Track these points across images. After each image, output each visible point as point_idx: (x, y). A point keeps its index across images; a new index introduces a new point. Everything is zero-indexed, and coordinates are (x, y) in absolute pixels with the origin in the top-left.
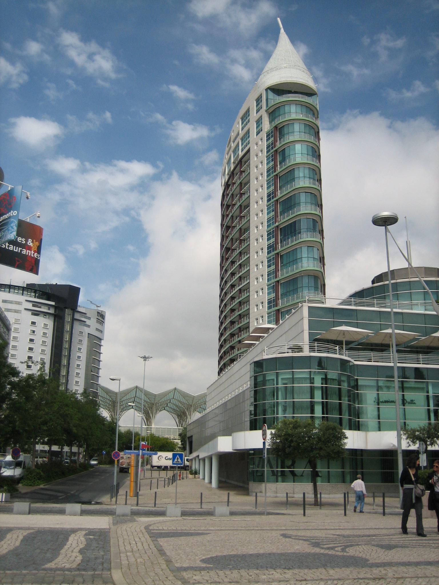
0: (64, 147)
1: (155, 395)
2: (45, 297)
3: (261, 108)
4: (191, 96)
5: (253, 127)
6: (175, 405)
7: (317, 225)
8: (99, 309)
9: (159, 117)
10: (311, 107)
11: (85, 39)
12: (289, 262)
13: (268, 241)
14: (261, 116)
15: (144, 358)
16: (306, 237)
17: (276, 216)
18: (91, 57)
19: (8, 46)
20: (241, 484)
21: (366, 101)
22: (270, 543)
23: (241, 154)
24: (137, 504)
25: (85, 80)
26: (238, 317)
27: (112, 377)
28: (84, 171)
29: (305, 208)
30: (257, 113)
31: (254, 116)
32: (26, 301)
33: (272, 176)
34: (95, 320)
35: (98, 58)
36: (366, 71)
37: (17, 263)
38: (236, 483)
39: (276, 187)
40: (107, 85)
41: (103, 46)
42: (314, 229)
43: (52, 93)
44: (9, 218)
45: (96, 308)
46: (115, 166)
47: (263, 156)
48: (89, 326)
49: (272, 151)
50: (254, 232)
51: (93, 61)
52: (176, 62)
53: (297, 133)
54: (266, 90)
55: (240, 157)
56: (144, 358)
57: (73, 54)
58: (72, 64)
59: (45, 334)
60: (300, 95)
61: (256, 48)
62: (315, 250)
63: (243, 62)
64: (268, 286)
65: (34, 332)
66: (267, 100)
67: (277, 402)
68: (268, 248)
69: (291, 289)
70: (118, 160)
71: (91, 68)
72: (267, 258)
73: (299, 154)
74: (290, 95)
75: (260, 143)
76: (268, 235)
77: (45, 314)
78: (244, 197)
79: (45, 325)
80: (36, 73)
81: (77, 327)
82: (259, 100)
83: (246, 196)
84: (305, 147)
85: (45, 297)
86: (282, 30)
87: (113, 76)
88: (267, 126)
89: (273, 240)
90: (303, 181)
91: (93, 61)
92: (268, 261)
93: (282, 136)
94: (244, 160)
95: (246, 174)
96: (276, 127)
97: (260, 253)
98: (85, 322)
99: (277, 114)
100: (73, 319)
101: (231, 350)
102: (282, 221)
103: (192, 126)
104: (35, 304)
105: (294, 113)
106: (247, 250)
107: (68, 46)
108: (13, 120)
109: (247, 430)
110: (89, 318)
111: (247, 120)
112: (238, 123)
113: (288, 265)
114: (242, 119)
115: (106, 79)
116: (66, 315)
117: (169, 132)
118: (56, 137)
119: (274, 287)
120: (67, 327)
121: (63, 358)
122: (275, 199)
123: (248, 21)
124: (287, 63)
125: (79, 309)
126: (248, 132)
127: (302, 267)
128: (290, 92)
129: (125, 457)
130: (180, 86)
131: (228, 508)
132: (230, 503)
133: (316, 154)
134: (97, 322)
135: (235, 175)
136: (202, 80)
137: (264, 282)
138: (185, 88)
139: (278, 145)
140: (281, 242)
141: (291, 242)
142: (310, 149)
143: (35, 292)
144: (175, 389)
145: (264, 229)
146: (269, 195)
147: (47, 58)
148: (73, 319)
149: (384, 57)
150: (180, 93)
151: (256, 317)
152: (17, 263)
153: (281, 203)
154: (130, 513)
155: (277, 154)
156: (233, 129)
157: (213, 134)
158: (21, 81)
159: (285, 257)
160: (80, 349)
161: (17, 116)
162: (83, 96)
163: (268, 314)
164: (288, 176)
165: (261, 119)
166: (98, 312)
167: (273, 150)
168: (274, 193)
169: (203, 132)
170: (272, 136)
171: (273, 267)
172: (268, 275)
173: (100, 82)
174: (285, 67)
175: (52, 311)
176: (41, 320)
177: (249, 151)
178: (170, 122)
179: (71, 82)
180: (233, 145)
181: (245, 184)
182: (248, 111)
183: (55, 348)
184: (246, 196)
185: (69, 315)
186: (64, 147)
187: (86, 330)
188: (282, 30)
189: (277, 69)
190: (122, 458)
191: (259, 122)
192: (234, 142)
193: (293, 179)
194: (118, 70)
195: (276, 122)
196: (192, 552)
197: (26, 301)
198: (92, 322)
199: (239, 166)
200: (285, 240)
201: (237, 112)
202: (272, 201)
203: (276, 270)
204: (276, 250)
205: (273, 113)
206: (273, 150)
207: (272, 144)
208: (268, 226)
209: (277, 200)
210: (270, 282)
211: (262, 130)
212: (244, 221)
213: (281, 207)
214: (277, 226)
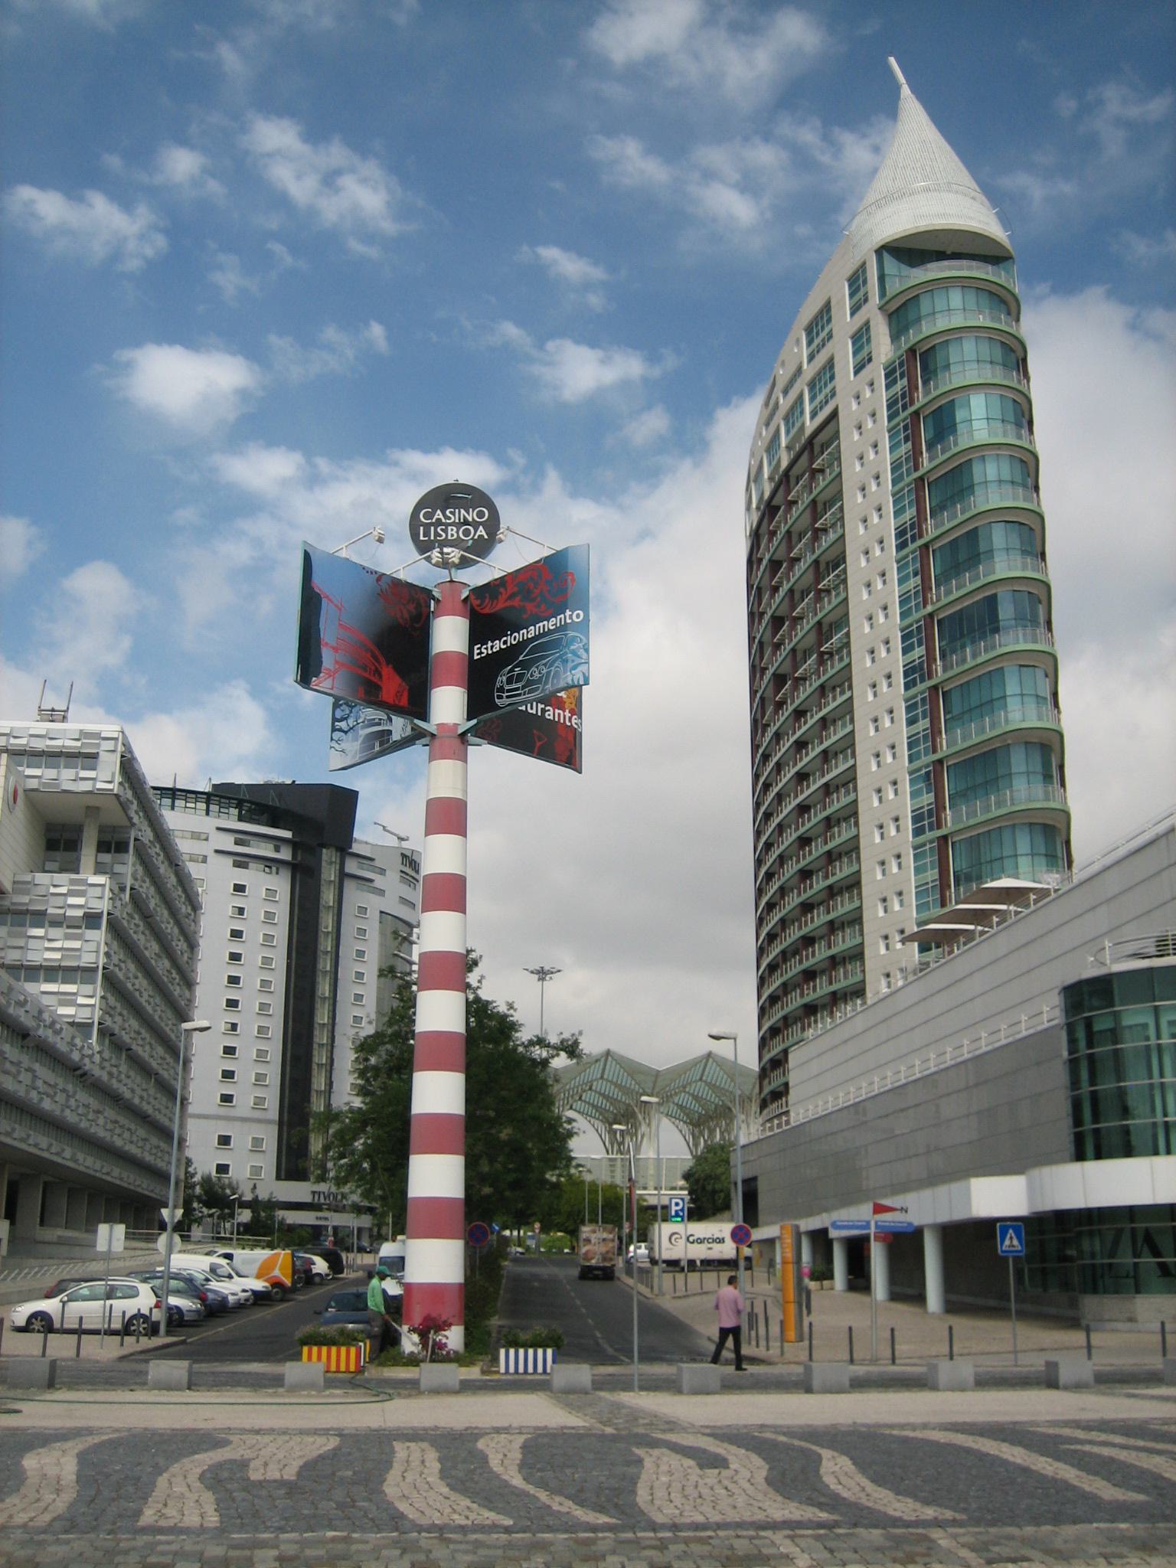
0: (259, 422)
1: (658, 1074)
2: (265, 817)
3: (866, 300)
4: (598, 273)
5: (844, 352)
6: (603, 1095)
7: (1036, 603)
8: (404, 844)
9: (511, 331)
10: (1003, 293)
11: (315, 135)
12: (970, 710)
13: (904, 653)
14: (867, 324)
15: (538, 972)
16: (1013, 641)
17: (925, 587)
18: (330, 180)
19: (114, 162)
20: (992, 1303)
21: (1080, 261)
22: (472, 1472)
23: (810, 426)
24: (852, 1361)
25: (315, 242)
26: (824, 858)
27: (714, 1033)
28: (313, 480)
29: (1005, 564)
30: (852, 314)
31: (844, 322)
32: (219, 829)
33: (907, 480)
34: (397, 876)
35: (347, 181)
36: (1067, 188)
37: (538, 744)
38: (969, 1299)
39: (920, 511)
40: (373, 252)
41: (363, 151)
42: (1034, 622)
43: (230, 279)
44: (563, 628)
45: (393, 842)
46: (396, 464)
47: (880, 428)
48: (381, 892)
49: (903, 415)
50: (860, 631)
51: (337, 190)
52: (557, 185)
53: (968, 366)
54: (880, 251)
55: (808, 432)
56: (538, 972)
57: (283, 175)
58: (281, 201)
59: (269, 915)
60: (964, 262)
61: (767, 137)
62: (1040, 674)
63: (736, 177)
64: (911, 773)
65: (241, 911)
66: (882, 278)
67: (1162, 1084)
68: (906, 674)
69: (979, 780)
70: (403, 449)
71: (331, 210)
72: (906, 701)
73: (979, 422)
74: (946, 263)
75: (868, 394)
76: (904, 638)
77: (269, 863)
78: (826, 541)
79: (269, 894)
80: (188, 231)
81: (354, 897)
82: (856, 281)
83: (832, 536)
84: (996, 402)
85: (265, 817)
86: (906, 91)
87: (389, 227)
88: (883, 348)
89: (919, 652)
90: (992, 493)
91: (337, 190)
92: (909, 709)
93: (929, 373)
94: (818, 441)
95: (829, 478)
96: (912, 351)
97: (884, 687)
98: (371, 881)
99: (912, 316)
100: (343, 875)
101: (806, 947)
102: (944, 601)
103: (599, 353)
104: (242, 838)
105: (952, 312)
106: (844, 680)
107: (270, 155)
108: (125, 355)
109: (1063, 1161)
110: (382, 872)
111: (823, 334)
112: (798, 342)
113: (966, 717)
114: (809, 330)
115: (370, 237)
116: (324, 864)
117: (537, 370)
118: (243, 394)
119: (930, 777)
120: (328, 897)
121: (320, 979)
122: (920, 542)
123: (748, 68)
124: (918, 180)
125: (356, 848)
126: (830, 364)
127: (1007, 721)
128: (941, 256)
129: (593, 1237)
130: (566, 247)
131: (1090, 1363)
132: (1093, 1351)
133: (1022, 415)
134: (403, 880)
135: (792, 481)
136: (629, 231)
137: (899, 765)
138: (581, 254)
139: (921, 399)
140: (943, 656)
141: (974, 657)
142: (1010, 404)
143: (239, 805)
144: (608, 1053)
145: (892, 624)
146: (901, 533)
147: (214, 187)
148: (343, 875)
149: (1114, 144)
150: (567, 265)
151: (880, 858)
152: (538, 744)
153: (938, 554)
154: (1091, 1379)
155: (922, 422)
156: (782, 357)
157: (656, 372)
158: (149, 252)
159: (955, 698)
160: (361, 953)
161: (138, 344)
162: (318, 280)
163: (915, 848)
164: (955, 482)
165: (868, 329)
166: (403, 856)
167: (906, 413)
168: (918, 524)
169: (630, 366)
170: (902, 376)
171: (924, 724)
172: (910, 746)
173: (356, 246)
174: (927, 190)
175: (285, 854)
176: (257, 880)
177: (834, 414)
178: (541, 346)
179: (277, 247)
180: (785, 403)
181: (827, 506)
182: (827, 307)
183: (297, 952)
184: (832, 536)
185: (331, 863)
186: (259, 422)
187: (375, 904)
188: (906, 91)
189: (901, 195)
190: (588, 1241)
191: (861, 337)
192: (785, 392)
193: (971, 488)
194: (401, 212)
195: (912, 337)
196: (712, 1488)
197: (219, 829)
198: (390, 882)
199: (805, 457)
200: (954, 652)
201: (795, 312)
202: (911, 547)
203: (934, 732)
204: (930, 677)
205: (901, 314)
206: (906, 413)
207: (903, 396)
208: (904, 615)
209: (926, 546)
210: (917, 764)
211: (870, 360)
212: (828, 604)
213: (938, 563)
214: (931, 615)
